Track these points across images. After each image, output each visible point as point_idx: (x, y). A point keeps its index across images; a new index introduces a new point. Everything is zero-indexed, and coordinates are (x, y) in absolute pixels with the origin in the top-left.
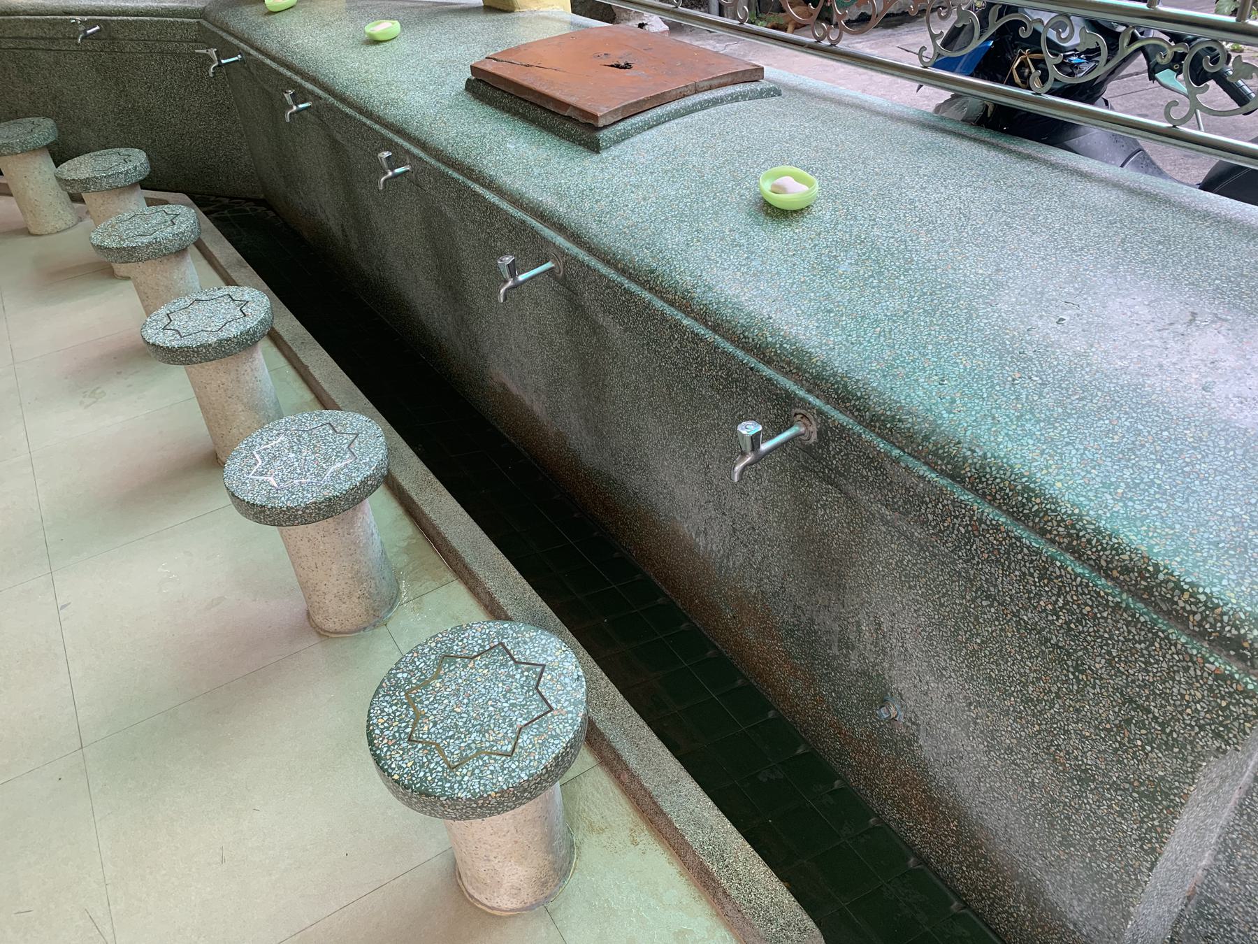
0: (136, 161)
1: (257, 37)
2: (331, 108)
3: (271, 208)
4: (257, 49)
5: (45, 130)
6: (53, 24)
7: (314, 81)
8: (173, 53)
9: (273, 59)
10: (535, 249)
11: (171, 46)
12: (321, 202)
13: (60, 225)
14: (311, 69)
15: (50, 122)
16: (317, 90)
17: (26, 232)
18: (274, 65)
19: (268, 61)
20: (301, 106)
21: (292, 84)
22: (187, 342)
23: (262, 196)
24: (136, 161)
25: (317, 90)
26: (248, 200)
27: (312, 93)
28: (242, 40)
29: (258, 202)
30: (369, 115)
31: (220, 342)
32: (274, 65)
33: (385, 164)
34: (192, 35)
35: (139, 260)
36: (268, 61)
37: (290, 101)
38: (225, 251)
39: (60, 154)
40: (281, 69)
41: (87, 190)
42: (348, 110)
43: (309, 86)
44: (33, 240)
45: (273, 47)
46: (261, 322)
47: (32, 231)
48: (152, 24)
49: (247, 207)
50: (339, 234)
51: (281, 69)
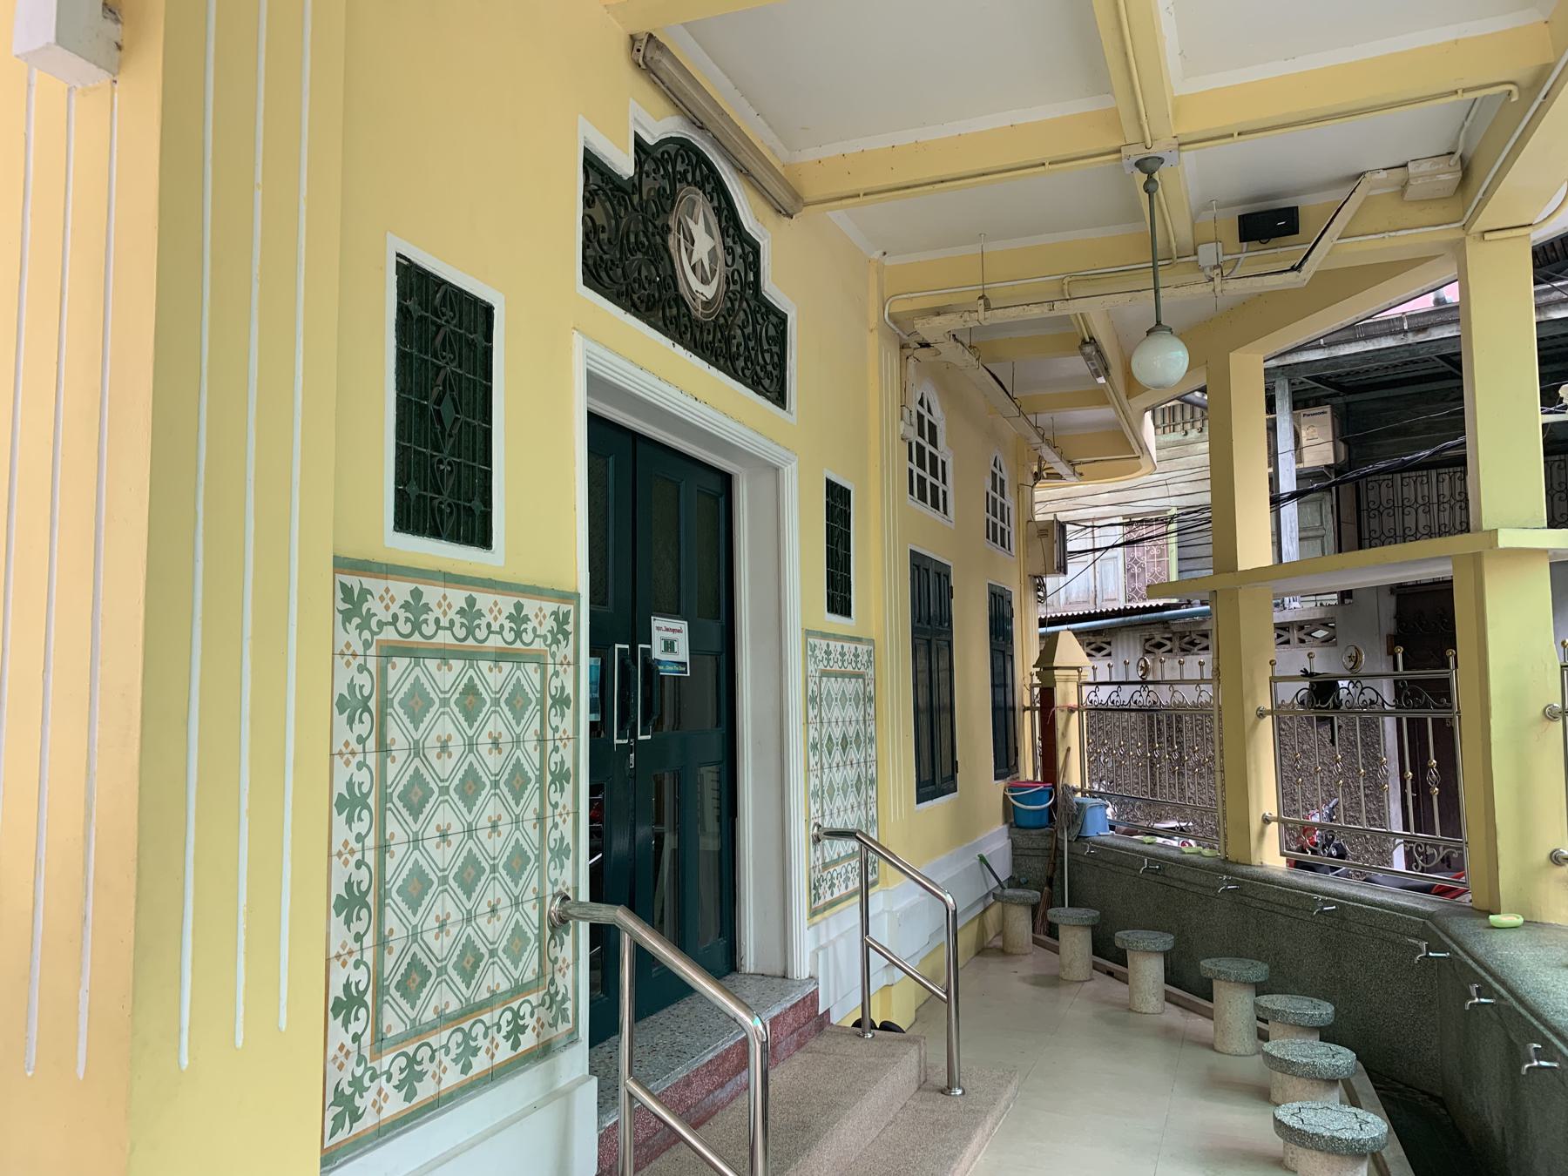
0: (1324, 1011)
1: (1470, 942)
2: (1510, 1009)
3: (1444, 1106)
4: (1465, 951)
5: (1259, 971)
6: (1299, 897)
7: (1503, 984)
8: (1393, 942)
9: (1475, 961)
10: (1485, 990)
11: (1393, 936)
12: (1488, 1103)
13: (1241, 1050)
14: (1505, 973)
15: (1266, 967)
16: (1503, 991)
17: (1212, 1047)
18: (1474, 965)
19: (1470, 962)
20: (1544, 1063)
21: (1481, 980)
22: (1307, 1128)
23: (1439, 1094)
24: (1324, 1011)
25: (1503, 991)
26: (1423, 1092)
27: (1497, 992)
28: (1455, 942)
29: (1433, 1097)
30: (1538, 1017)
31: (1333, 1138)
32: (1474, 965)
33: (1532, 1053)
34: (1415, 931)
35: (1294, 1074)
36: (1470, 962)
37: (1474, 993)
38: (1364, 1085)
39: (1261, 989)
40: (1479, 970)
41: (1274, 1019)
42: (1522, 1011)
43: (1497, 986)
44: (1215, 1055)
45: (1479, 950)
46: (1373, 1139)
47: (1218, 1047)
48: (1381, 914)
49: (1420, 1097)
50: (1499, 1139)
51: (1479, 970)
